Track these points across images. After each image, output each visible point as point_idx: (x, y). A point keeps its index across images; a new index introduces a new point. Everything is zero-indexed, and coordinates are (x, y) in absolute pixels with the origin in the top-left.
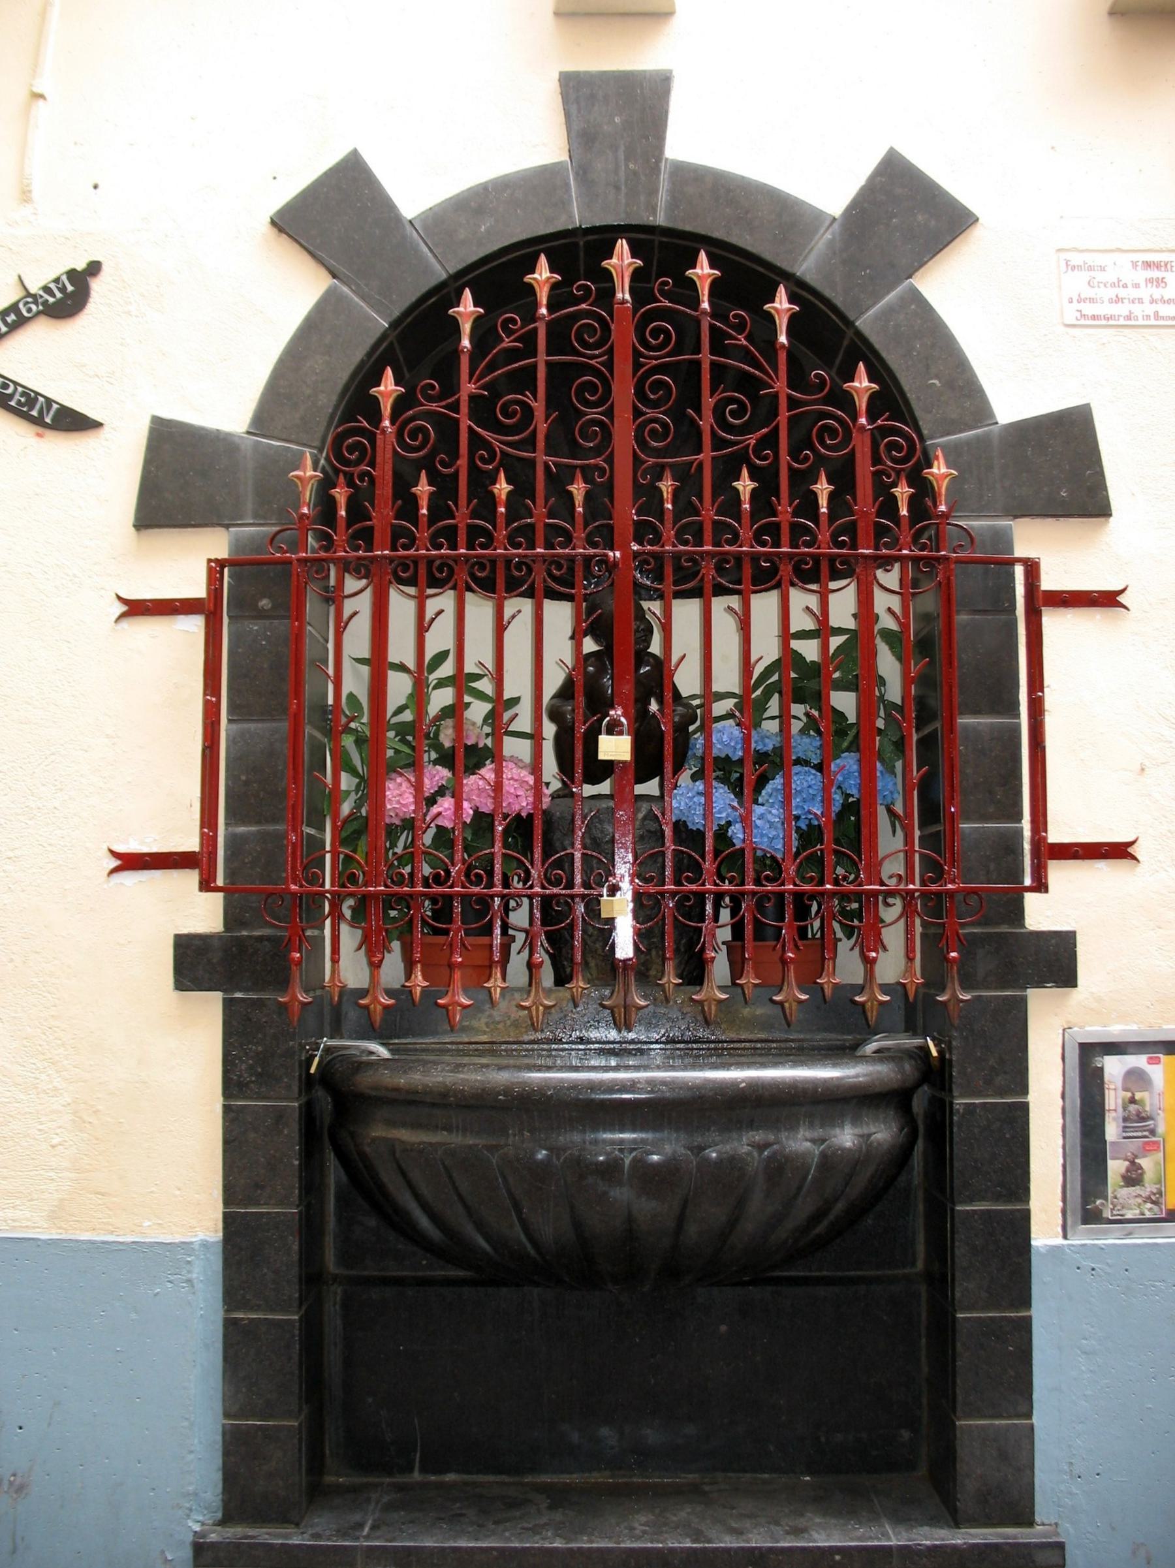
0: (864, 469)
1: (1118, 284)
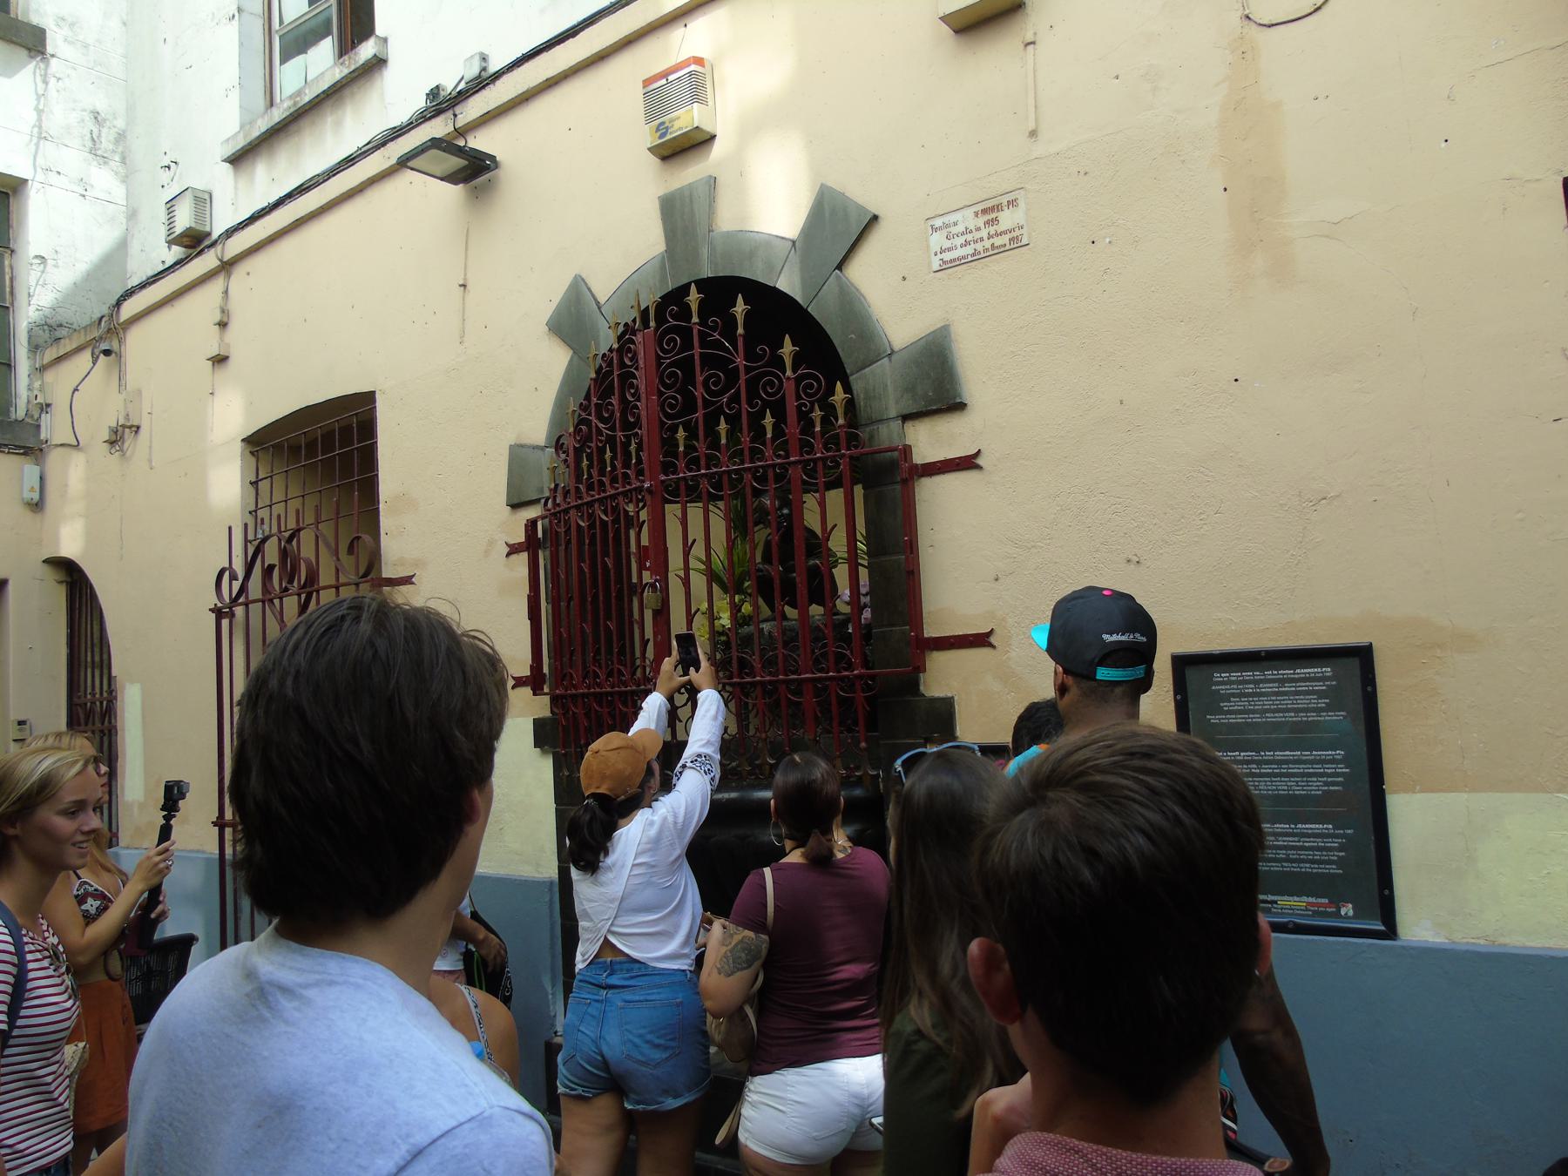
0: (791, 404)
1: (967, 231)
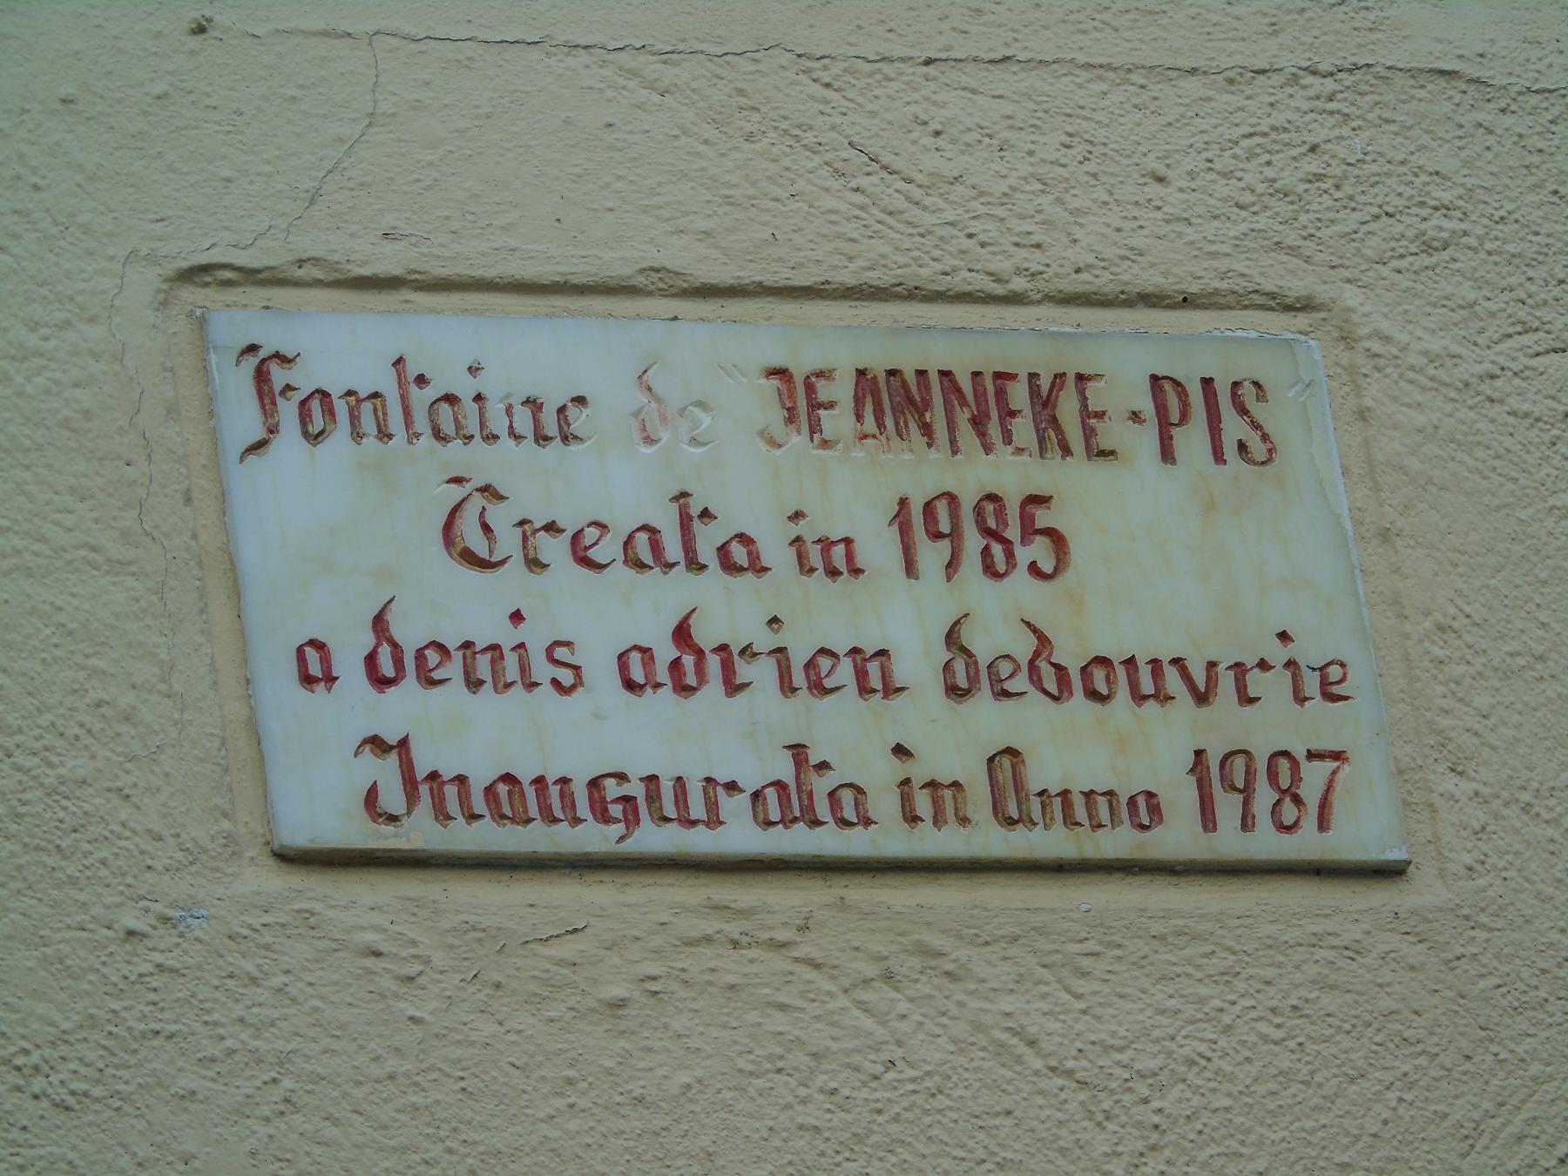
1: (681, 539)
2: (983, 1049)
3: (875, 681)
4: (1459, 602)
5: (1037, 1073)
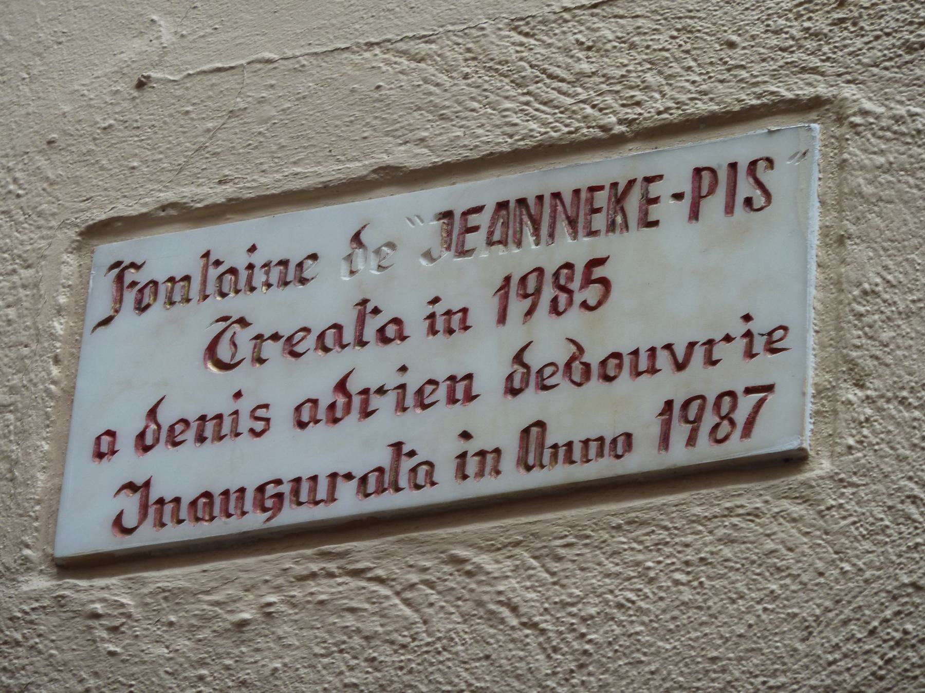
2: (481, 618)
3: (460, 394)
4: (884, 273)
5: (513, 628)
